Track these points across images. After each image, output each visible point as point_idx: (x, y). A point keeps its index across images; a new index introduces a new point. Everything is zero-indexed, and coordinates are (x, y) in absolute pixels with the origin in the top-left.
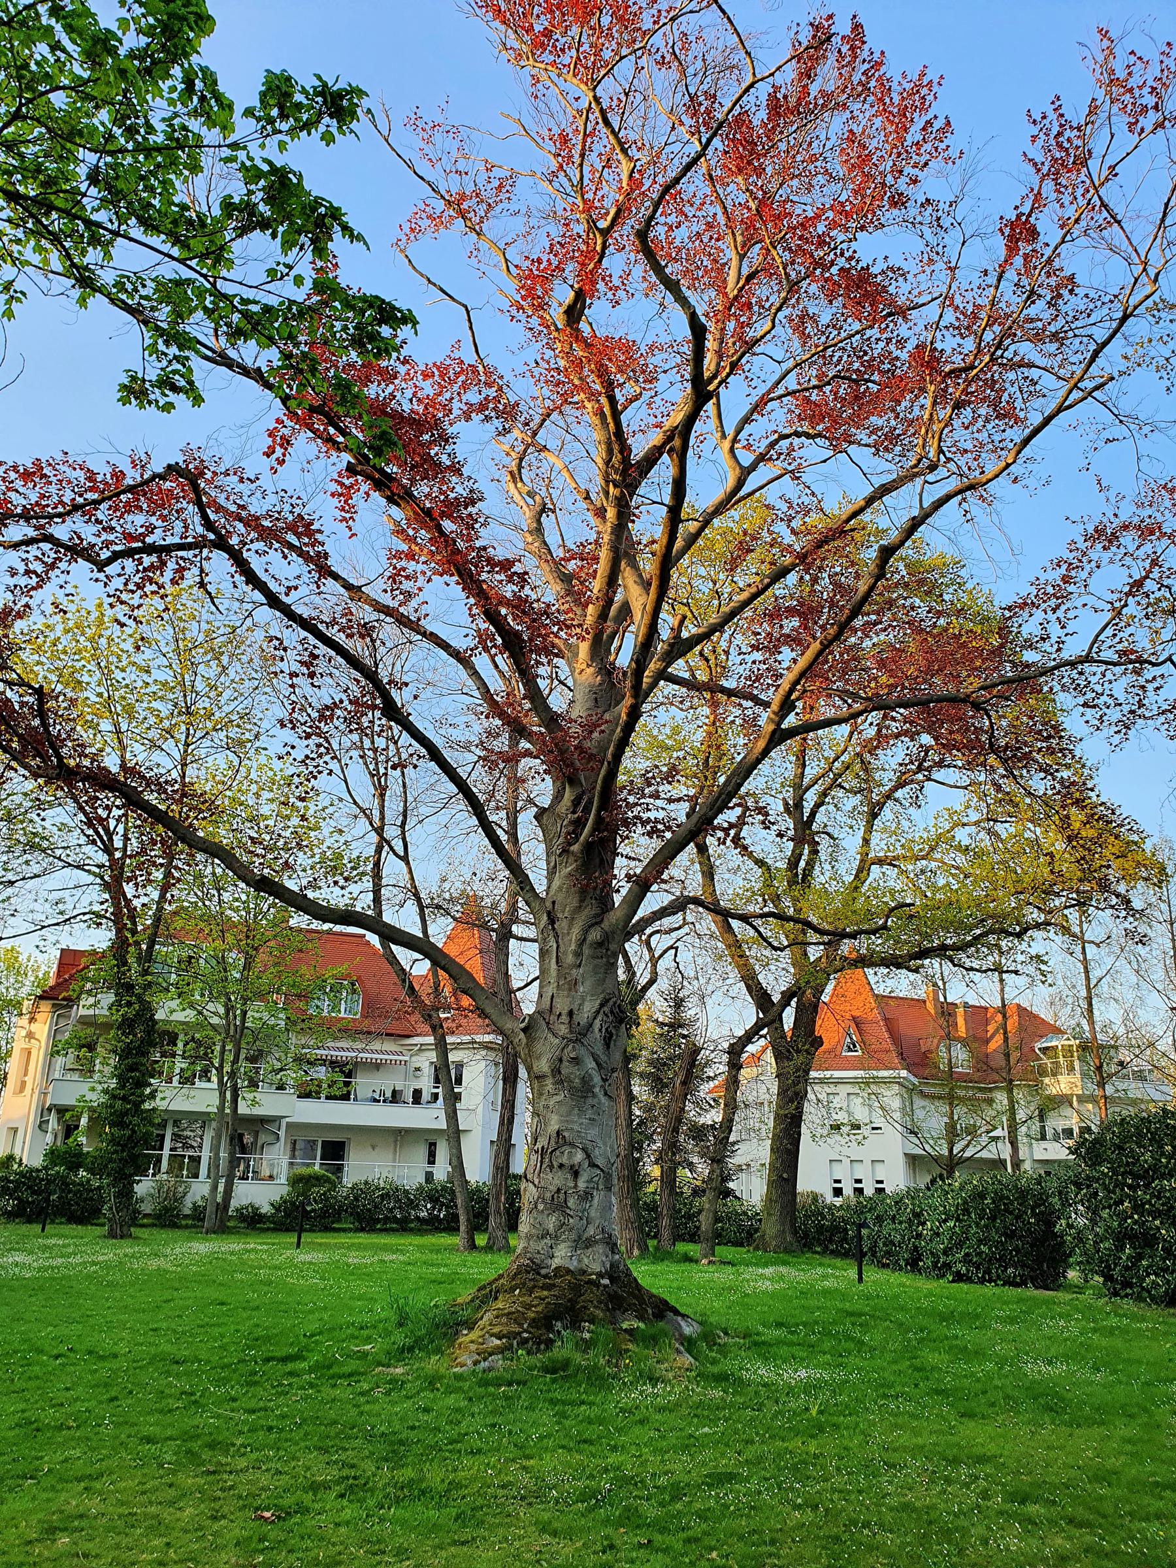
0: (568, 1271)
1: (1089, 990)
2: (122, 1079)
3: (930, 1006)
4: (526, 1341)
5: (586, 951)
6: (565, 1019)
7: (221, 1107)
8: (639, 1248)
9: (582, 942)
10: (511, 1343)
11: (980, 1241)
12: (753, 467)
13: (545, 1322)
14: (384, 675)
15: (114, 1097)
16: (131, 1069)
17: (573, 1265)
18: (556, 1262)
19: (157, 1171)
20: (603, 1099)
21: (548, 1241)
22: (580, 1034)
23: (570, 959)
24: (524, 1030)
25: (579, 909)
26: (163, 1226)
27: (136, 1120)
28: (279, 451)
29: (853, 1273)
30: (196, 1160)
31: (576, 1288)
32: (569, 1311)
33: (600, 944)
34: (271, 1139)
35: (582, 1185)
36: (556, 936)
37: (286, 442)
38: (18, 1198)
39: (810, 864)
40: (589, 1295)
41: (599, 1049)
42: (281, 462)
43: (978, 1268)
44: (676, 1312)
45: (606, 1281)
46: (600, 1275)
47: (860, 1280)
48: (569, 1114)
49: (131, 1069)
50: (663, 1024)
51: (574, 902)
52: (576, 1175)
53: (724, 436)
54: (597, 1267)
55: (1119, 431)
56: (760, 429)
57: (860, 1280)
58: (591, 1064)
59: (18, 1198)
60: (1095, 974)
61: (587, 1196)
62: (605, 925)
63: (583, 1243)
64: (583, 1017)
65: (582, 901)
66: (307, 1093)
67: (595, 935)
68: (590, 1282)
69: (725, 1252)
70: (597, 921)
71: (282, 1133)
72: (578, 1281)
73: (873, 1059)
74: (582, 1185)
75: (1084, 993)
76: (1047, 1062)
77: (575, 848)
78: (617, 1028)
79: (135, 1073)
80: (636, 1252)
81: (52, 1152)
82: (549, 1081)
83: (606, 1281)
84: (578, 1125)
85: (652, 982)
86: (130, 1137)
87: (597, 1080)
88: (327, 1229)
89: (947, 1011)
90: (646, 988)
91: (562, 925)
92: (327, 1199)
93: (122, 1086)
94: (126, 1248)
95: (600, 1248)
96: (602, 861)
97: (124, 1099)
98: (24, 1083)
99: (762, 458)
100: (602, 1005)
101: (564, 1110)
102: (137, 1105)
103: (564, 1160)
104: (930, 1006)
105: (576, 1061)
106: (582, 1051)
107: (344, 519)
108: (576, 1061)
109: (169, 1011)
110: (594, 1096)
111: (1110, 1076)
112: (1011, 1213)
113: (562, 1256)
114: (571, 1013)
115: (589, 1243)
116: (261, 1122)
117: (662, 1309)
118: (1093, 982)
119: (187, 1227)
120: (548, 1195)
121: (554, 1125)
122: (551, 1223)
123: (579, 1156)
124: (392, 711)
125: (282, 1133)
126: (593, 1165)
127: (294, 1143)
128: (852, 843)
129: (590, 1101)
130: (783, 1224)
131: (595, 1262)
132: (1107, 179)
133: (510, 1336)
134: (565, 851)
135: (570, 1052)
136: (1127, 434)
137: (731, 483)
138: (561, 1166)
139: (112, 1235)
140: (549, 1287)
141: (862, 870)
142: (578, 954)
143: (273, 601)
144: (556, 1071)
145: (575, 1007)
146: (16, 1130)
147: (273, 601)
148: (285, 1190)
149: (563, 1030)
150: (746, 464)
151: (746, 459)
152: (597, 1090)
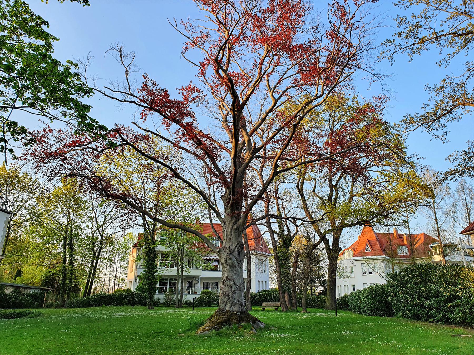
0: (229, 311)
1: (438, 228)
2: (148, 268)
3: (395, 235)
4: (216, 328)
5: (233, 231)
6: (228, 248)
7: (178, 273)
8: (286, 308)
9: (232, 229)
10: (211, 328)
11: (371, 304)
12: (279, 98)
13: (221, 324)
14: (173, 168)
15: (146, 272)
16: (150, 265)
17: (231, 310)
18: (227, 309)
19: (166, 291)
20: (238, 268)
21: (224, 304)
22: (231, 252)
23: (229, 233)
24: (218, 252)
25: (231, 220)
26: (165, 306)
27: (152, 278)
28: (144, 117)
29: (335, 314)
30: (166, 288)
31: (231, 316)
32: (228, 321)
33: (236, 229)
34: (197, 282)
35: (233, 290)
36: (226, 228)
37: (145, 115)
38: (128, 300)
39: (336, 197)
40: (234, 317)
41: (237, 255)
42: (145, 120)
43: (372, 311)
44: (259, 321)
45: (239, 314)
46: (237, 312)
47: (336, 315)
48: (229, 272)
49: (150, 265)
50: (305, 246)
51: (230, 219)
52: (231, 287)
53: (271, 91)
54: (236, 310)
55: (375, 79)
56: (282, 87)
57: (336, 315)
58: (235, 260)
59: (128, 300)
60: (439, 224)
61: (234, 292)
62: (238, 224)
63: (233, 304)
64: (232, 248)
65: (232, 218)
66: (205, 269)
67: (235, 227)
68: (234, 314)
69: (309, 309)
70: (235, 223)
71: (199, 280)
72: (231, 314)
73: (375, 252)
74: (233, 290)
75: (437, 230)
76: (433, 251)
77: (229, 205)
78: (242, 250)
79: (151, 266)
80: (285, 310)
81: (137, 287)
82: (225, 264)
83: (239, 314)
84: (232, 274)
85: (296, 233)
86: (151, 283)
87: (236, 263)
88: (210, 306)
89: (400, 236)
90: (294, 236)
91: (227, 225)
92: (209, 298)
93: (148, 269)
94: (150, 311)
95: (238, 305)
96: (237, 208)
97: (149, 273)
98: (132, 269)
99: (281, 96)
100: (237, 245)
101: (228, 271)
102: (153, 274)
103: (228, 284)
104: (395, 235)
105: (230, 259)
106: (232, 256)
107: (167, 129)
108: (230, 259)
109: (160, 248)
110: (236, 267)
111: (447, 255)
112: (380, 296)
113: (228, 307)
114: (229, 247)
115: (235, 304)
116: (194, 277)
117: (255, 321)
118: (439, 226)
119: (172, 306)
120: (224, 293)
121: (226, 275)
122: (225, 299)
123: (232, 283)
124: (177, 176)
125: (199, 280)
126: (235, 285)
127: (204, 283)
128: (348, 190)
129: (235, 269)
130: (332, 301)
131: (236, 309)
132: (352, 18)
133: (213, 327)
134: (227, 206)
135: (229, 257)
136: (378, 79)
137: (272, 103)
138: (228, 285)
139: (149, 308)
140: (223, 315)
141: (351, 198)
142: (231, 232)
143: (143, 154)
144: (226, 262)
145: (231, 246)
146: (131, 282)
147: (143, 154)
148: (199, 296)
149: (227, 251)
150: (277, 98)
151: (277, 96)
152: (236, 266)
